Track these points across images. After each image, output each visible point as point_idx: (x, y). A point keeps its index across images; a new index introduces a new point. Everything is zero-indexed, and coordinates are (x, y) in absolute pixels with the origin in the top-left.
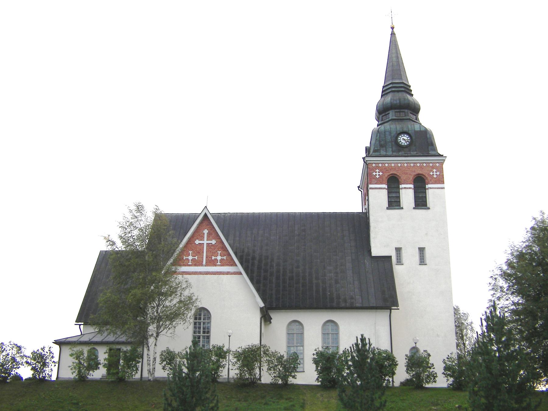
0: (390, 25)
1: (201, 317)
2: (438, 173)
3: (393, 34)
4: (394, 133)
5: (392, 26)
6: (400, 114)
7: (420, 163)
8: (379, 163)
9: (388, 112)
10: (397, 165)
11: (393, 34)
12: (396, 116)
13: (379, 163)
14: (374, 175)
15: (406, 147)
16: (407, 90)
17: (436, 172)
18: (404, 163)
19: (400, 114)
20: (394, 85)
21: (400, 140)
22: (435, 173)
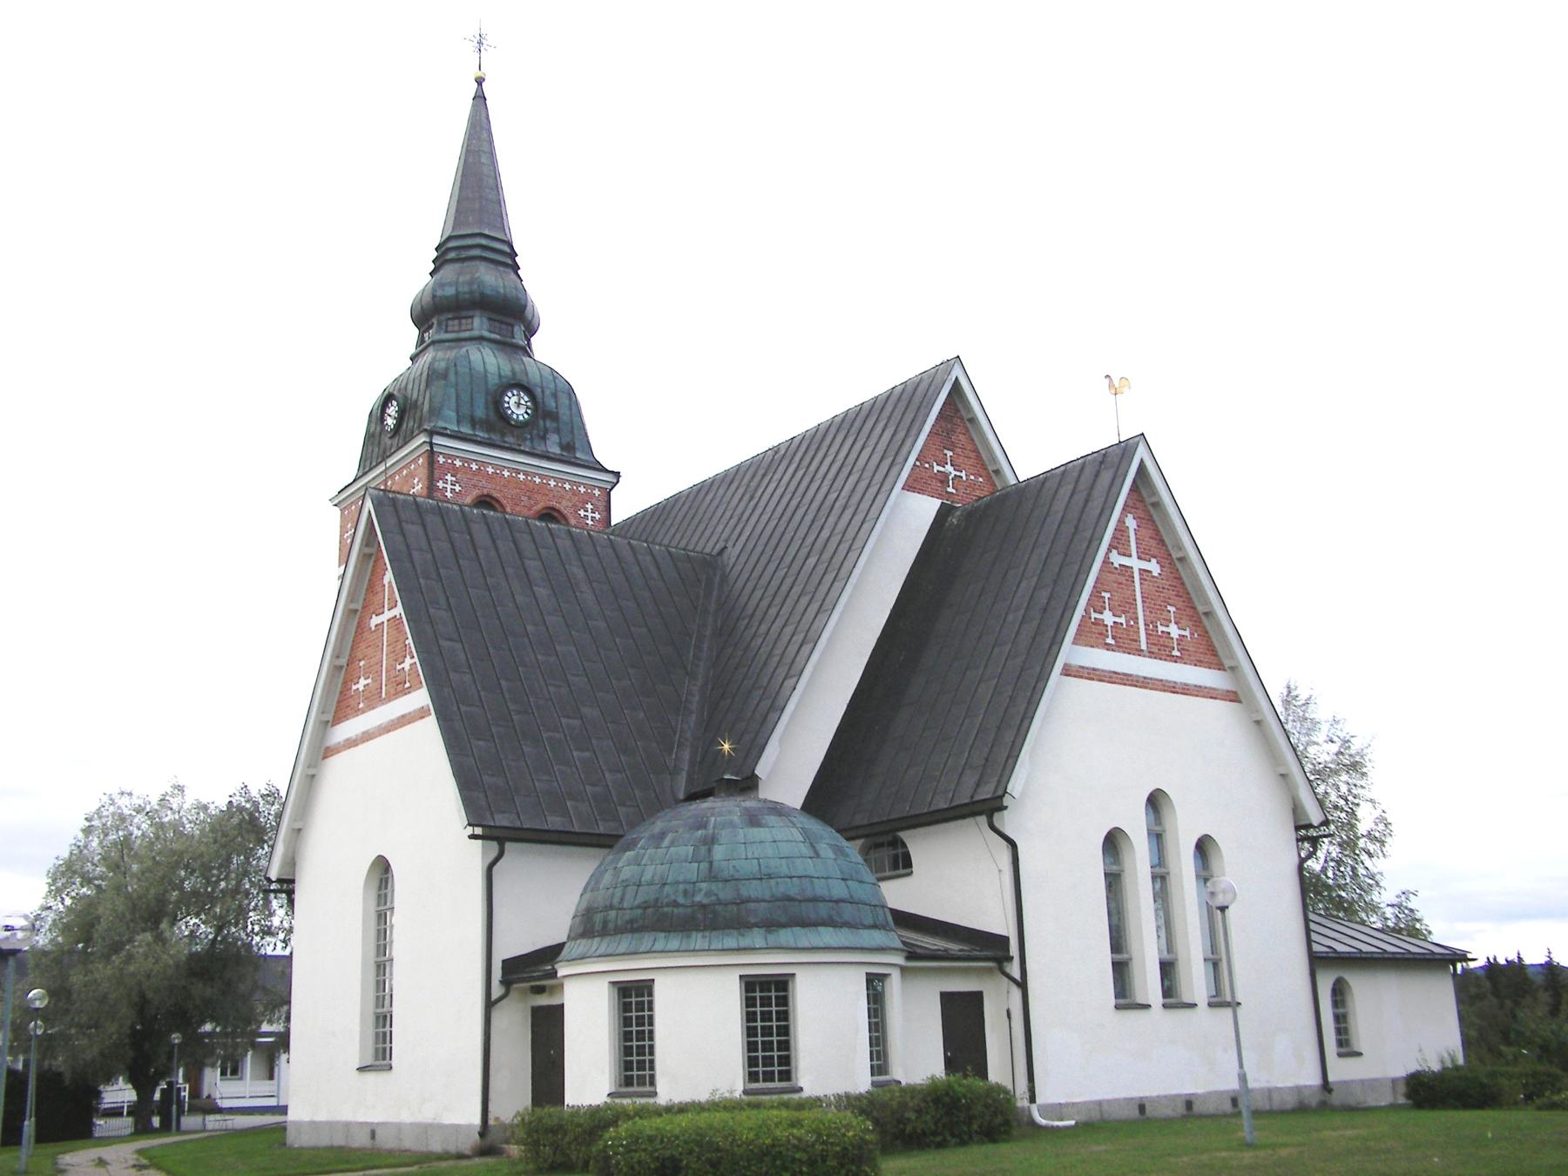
0: (475, 73)
1: (774, 1081)
2: (589, 522)
3: (480, 98)
4: (493, 380)
5: (480, 74)
6: (460, 324)
7: (463, 459)
8: (535, 475)
9: (470, 313)
10: (463, 465)
11: (480, 98)
12: (490, 332)
13: (535, 475)
14: (457, 485)
15: (525, 424)
16: (507, 259)
17: (452, 484)
18: (518, 472)
19: (460, 324)
20: (484, 242)
21: (508, 403)
22: (449, 487)
